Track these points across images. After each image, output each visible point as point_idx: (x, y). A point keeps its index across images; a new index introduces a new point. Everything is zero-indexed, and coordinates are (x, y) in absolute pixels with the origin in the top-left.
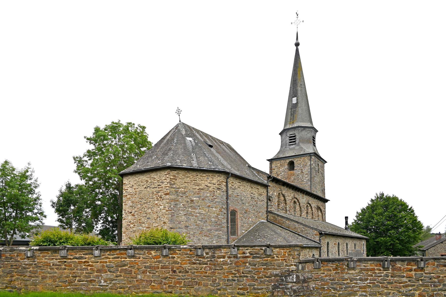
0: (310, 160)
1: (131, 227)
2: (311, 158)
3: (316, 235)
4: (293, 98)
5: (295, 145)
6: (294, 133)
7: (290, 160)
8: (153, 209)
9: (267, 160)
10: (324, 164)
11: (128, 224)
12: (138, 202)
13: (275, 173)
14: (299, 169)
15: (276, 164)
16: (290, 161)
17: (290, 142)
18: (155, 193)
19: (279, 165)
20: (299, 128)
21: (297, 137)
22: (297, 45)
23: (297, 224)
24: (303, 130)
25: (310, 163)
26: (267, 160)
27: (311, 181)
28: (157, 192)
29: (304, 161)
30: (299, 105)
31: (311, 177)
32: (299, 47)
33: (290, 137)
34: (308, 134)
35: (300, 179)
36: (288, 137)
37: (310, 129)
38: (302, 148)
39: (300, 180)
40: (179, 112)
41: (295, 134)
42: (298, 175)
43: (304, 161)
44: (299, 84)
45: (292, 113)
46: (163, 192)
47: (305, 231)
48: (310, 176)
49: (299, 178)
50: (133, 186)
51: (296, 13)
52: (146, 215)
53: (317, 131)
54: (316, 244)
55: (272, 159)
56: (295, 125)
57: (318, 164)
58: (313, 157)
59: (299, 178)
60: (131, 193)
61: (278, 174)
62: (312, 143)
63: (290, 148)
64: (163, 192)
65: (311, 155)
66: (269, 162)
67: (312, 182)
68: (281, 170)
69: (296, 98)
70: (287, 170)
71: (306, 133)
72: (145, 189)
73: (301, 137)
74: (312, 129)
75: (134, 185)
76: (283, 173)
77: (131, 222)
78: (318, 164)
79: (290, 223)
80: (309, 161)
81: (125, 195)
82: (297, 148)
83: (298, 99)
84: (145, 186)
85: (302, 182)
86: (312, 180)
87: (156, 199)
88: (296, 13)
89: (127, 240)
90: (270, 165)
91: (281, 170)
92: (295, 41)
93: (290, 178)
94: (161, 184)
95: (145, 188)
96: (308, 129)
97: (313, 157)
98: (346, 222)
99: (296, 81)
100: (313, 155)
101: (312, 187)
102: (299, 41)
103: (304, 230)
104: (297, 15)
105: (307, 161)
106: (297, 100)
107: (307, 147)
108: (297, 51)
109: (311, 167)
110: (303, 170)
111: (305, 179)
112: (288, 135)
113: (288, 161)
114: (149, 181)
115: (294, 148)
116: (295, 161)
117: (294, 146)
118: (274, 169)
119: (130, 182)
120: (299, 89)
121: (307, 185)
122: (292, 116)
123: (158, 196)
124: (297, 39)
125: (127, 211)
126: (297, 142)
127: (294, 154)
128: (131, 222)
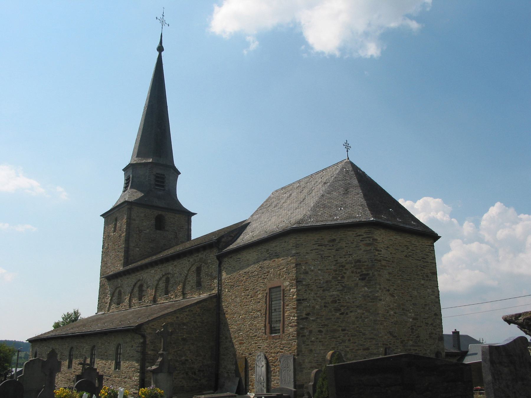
1: (390, 315)
7: (160, 213)
8: (419, 292)
9: (197, 214)
11: (386, 310)
12: (398, 276)
15: (138, 212)
18: (420, 268)
22: (160, 49)
26: (197, 214)
28: (422, 268)
32: (162, 53)
40: (347, 146)
46: (430, 270)
50: (388, 247)
52: (410, 299)
60: (387, 258)
64: (430, 270)
72: (406, 258)
75: (389, 247)
77: (389, 306)
81: (379, 259)
84: (405, 253)
87: (421, 277)
89: (386, 337)
91: (145, 224)
94: (425, 257)
95: (406, 256)
113: (156, 213)
114: (410, 248)
119: (384, 240)
123: (424, 273)
125: (382, 287)
128: (389, 306)
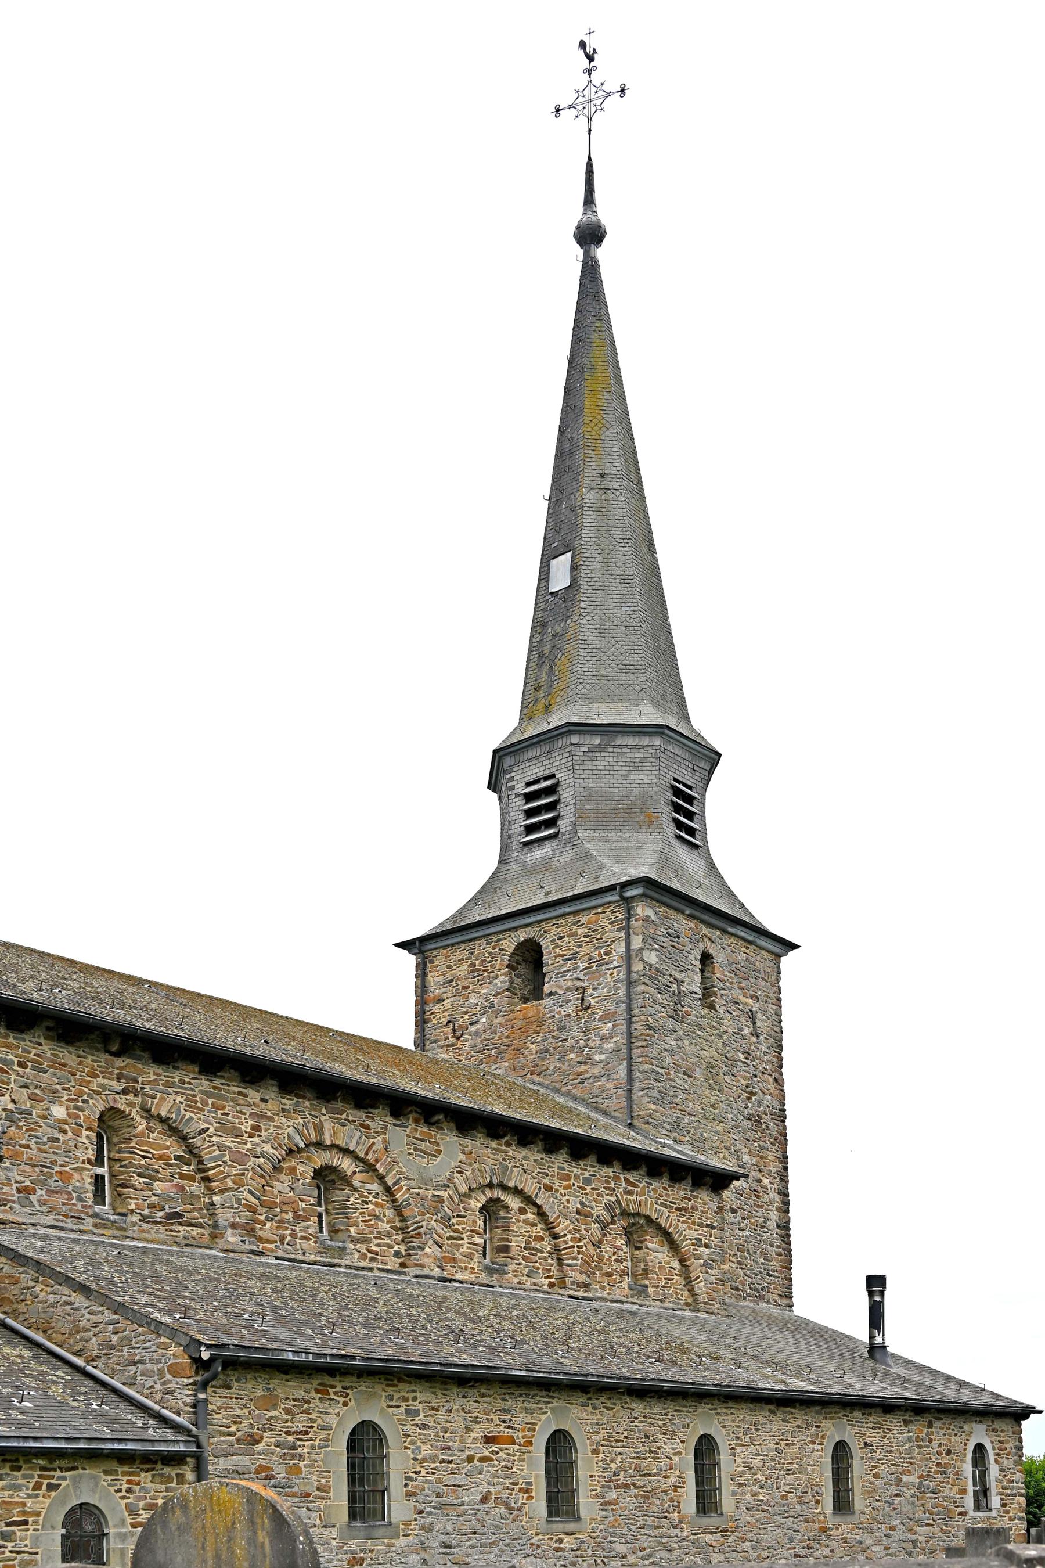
0: (627, 929)
2: (629, 915)
3: (174, 1370)
4: (554, 562)
5: (555, 843)
6: (547, 773)
7: (522, 935)
9: (398, 945)
10: (778, 956)
13: (444, 1021)
14: (568, 989)
16: (521, 945)
17: (530, 829)
19: (463, 970)
20: (575, 739)
21: (566, 794)
23: (87, 1303)
24: (594, 749)
25: (623, 944)
27: (630, 1059)
29: (594, 934)
30: (584, 598)
31: (630, 1034)
32: (602, 253)
33: (529, 797)
34: (636, 769)
35: (572, 1049)
36: (517, 795)
37: (646, 741)
38: (588, 856)
39: (572, 1056)
41: (553, 776)
42: (561, 1028)
43: (594, 934)
44: (588, 472)
45: (546, 650)
47: (121, 1344)
48: (624, 1028)
49: (570, 1043)
51: (583, 45)
53: (713, 758)
54: (169, 1434)
55: (423, 940)
56: (555, 721)
57: (706, 958)
58: (639, 910)
59: (570, 1043)
61: (460, 1026)
62: (660, 828)
63: (524, 865)
65: (628, 894)
66: (409, 961)
67: (635, 1067)
68: (473, 1000)
69: (569, 554)
70: (503, 1000)
71: (622, 767)
73: (588, 790)
74: (657, 741)
76: (484, 1020)
78: (706, 958)
79: (52, 1299)
80: (622, 934)
82: (566, 857)
83: (584, 562)
85: (583, 1068)
86: (636, 1052)
88: (583, 45)
90: (417, 976)
91: (473, 1000)
92: (575, 214)
93: (519, 1051)
96: (630, 741)
97: (642, 909)
98: (871, 1309)
99: (571, 453)
100: (643, 895)
101: (637, 1095)
102: (605, 214)
103: (115, 1338)
104: (590, 58)
105: (612, 933)
106: (574, 568)
107: (626, 850)
108: (590, 272)
109: (629, 972)
110: (590, 991)
111: (600, 1050)
112: (521, 789)
113: (509, 944)
115: (546, 865)
116: (545, 944)
117: (547, 849)
118: (441, 1000)
120: (588, 503)
121: (608, 1085)
122: (546, 668)
124: (589, 200)
126: (564, 825)
127: (540, 900)
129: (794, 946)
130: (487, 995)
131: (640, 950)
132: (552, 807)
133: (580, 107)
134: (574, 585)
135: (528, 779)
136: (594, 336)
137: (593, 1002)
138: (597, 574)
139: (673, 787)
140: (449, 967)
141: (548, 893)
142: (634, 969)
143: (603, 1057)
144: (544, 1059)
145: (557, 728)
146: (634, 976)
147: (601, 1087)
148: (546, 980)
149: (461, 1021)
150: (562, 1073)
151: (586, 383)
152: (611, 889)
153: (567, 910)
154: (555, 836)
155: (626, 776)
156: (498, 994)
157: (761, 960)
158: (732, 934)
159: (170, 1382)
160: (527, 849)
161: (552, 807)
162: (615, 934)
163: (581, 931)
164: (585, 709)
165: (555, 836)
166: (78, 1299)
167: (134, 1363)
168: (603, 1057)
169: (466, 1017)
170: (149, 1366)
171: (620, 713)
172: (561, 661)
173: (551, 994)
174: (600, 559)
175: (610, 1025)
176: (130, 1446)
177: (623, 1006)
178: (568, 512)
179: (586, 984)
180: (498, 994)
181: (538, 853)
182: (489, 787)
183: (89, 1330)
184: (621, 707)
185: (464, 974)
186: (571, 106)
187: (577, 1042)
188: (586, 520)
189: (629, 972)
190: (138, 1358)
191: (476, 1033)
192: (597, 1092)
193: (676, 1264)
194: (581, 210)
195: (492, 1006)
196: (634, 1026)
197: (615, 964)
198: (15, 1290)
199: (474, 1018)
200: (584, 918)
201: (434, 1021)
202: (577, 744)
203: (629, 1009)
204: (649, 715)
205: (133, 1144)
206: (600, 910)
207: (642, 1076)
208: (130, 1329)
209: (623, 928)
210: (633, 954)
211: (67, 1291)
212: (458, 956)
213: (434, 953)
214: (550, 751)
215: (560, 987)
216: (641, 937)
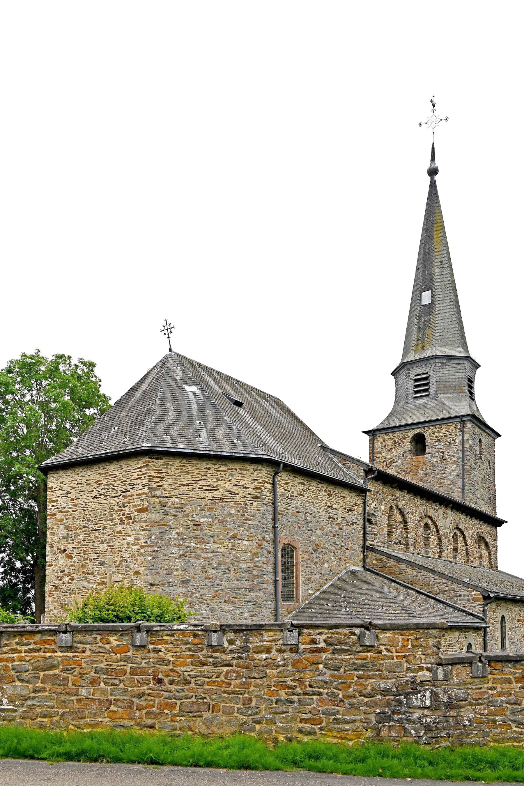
0: (462, 432)
2: (464, 426)
4: (423, 294)
5: (428, 398)
6: (425, 372)
7: (417, 431)
9: (363, 432)
10: (494, 439)
13: (382, 461)
14: (436, 452)
17: (416, 392)
19: (390, 442)
20: (437, 360)
21: (432, 380)
24: (443, 364)
25: (461, 437)
27: (463, 479)
30: (437, 308)
31: (463, 470)
32: (437, 178)
34: (458, 372)
35: (438, 474)
36: (411, 379)
37: (461, 362)
38: (443, 404)
39: (438, 476)
41: (427, 373)
45: (421, 326)
47: (450, 590)
48: (461, 467)
49: (437, 471)
51: (432, 101)
53: (477, 366)
56: (428, 353)
57: (480, 440)
58: (468, 425)
59: (437, 471)
61: (389, 463)
62: (465, 393)
63: (415, 405)
66: (367, 438)
67: (466, 482)
69: (430, 291)
70: (409, 455)
71: (453, 371)
73: (441, 379)
74: (465, 362)
79: (415, 574)
82: (433, 403)
83: (436, 294)
85: (443, 481)
86: (466, 477)
88: (432, 101)
92: (427, 165)
93: (415, 473)
96: (456, 362)
97: (469, 425)
99: (429, 253)
100: (470, 420)
102: (438, 163)
103: (447, 588)
104: (434, 106)
105: (455, 433)
106: (432, 296)
107: (456, 402)
108: (433, 186)
109: (463, 447)
110: (446, 453)
112: (412, 376)
113: (411, 434)
115: (425, 406)
116: (427, 435)
117: (424, 400)
118: (380, 453)
122: (421, 333)
126: (432, 391)
127: (425, 419)
129: (500, 436)
130: (401, 452)
131: (468, 440)
132: (427, 384)
133: (430, 124)
134: (433, 302)
135: (416, 374)
136: (436, 210)
137: (447, 457)
138: (441, 299)
139: (468, 378)
140: (384, 441)
141: (428, 417)
142: (465, 446)
143: (452, 477)
144: (426, 477)
145: (431, 356)
146: (465, 449)
147: (451, 488)
148: (427, 448)
149: (389, 461)
150: (434, 482)
151: (434, 228)
152: (458, 417)
153: (437, 423)
154: (428, 395)
155: (454, 374)
156: (406, 452)
157: (485, 439)
158: (486, 432)
159: (473, 603)
160: (415, 399)
161: (427, 384)
162: (457, 433)
163: (442, 431)
164: (440, 350)
165: (428, 395)
166: (429, 575)
167: (457, 596)
168: (452, 477)
169: (392, 460)
170: (463, 598)
171: (452, 352)
172: (428, 331)
173: (429, 453)
174: (442, 293)
175: (455, 466)
176: (460, 624)
177: (461, 459)
178: (429, 275)
179: (444, 450)
180: (406, 452)
181: (420, 401)
182: (393, 374)
183: (434, 585)
184: (452, 349)
185: (390, 444)
186: (426, 123)
187: (440, 471)
188: (437, 279)
189: (463, 447)
190: (458, 595)
191: (396, 466)
192: (449, 490)
193: (487, 554)
194: (430, 162)
195: (403, 456)
196: (465, 467)
197: (457, 444)
198: (398, 570)
199: (395, 460)
200: (444, 427)
201: (378, 460)
202: (438, 363)
203: (463, 461)
204: (459, 352)
205: (393, 518)
206: (451, 424)
207: (468, 485)
208: (454, 585)
209: (461, 431)
210: (465, 441)
211: (424, 572)
212: (388, 437)
213: (377, 436)
214: (427, 364)
215: (433, 451)
216: (468, 435)
